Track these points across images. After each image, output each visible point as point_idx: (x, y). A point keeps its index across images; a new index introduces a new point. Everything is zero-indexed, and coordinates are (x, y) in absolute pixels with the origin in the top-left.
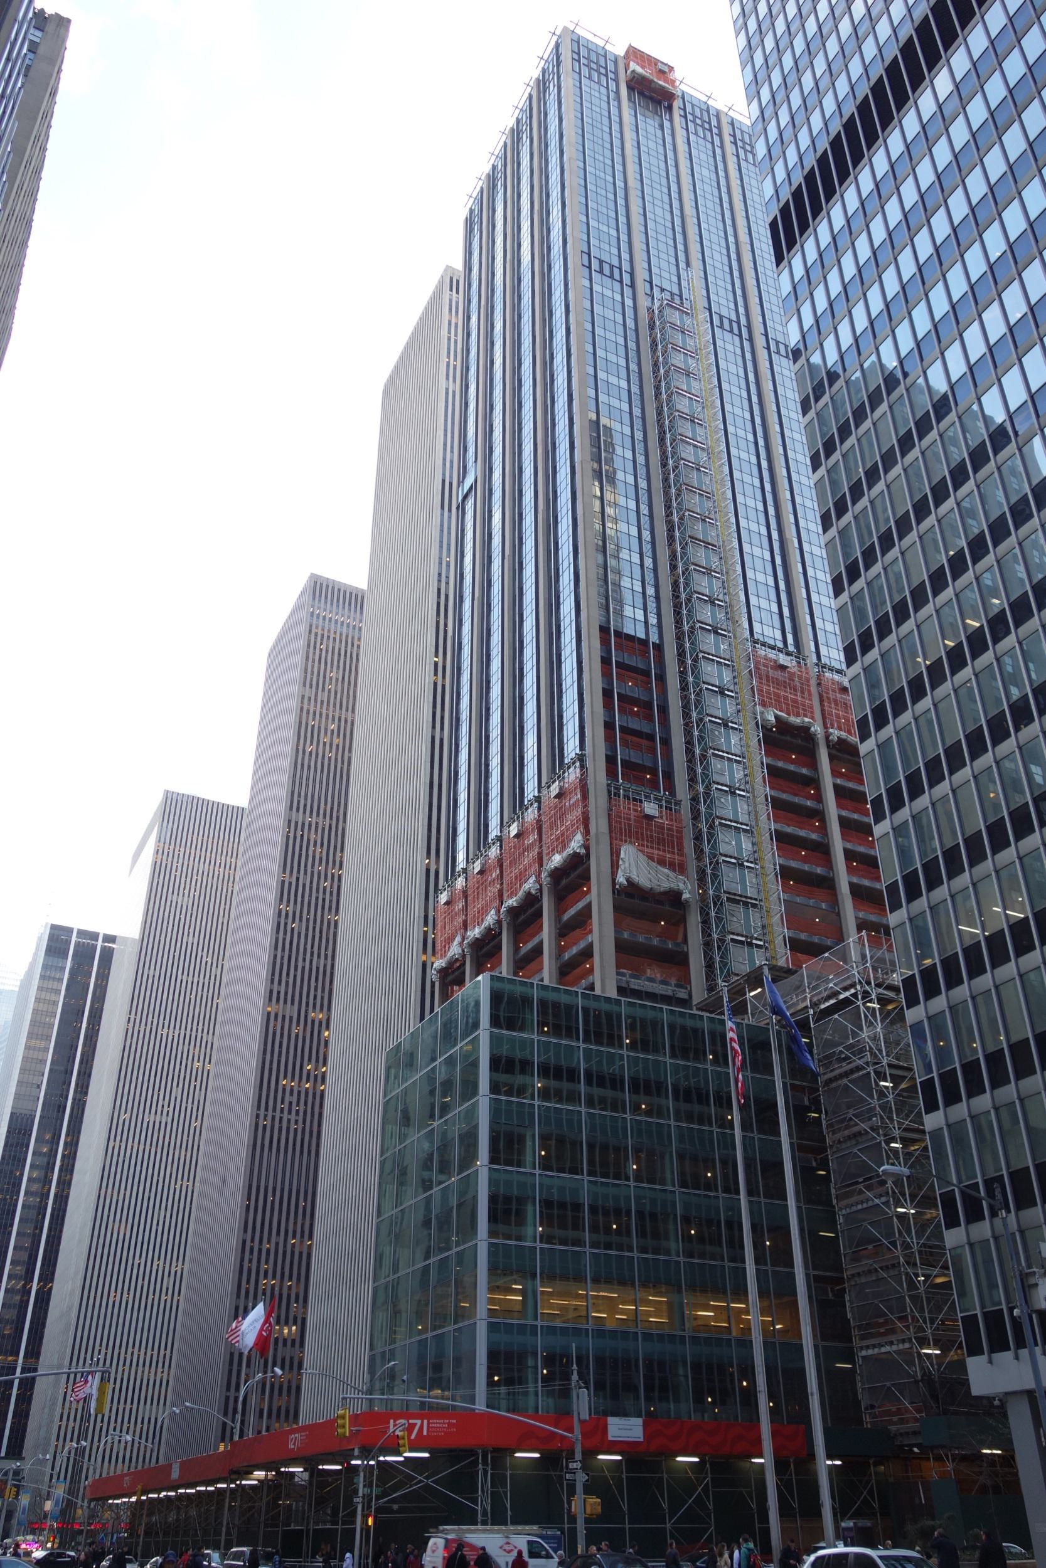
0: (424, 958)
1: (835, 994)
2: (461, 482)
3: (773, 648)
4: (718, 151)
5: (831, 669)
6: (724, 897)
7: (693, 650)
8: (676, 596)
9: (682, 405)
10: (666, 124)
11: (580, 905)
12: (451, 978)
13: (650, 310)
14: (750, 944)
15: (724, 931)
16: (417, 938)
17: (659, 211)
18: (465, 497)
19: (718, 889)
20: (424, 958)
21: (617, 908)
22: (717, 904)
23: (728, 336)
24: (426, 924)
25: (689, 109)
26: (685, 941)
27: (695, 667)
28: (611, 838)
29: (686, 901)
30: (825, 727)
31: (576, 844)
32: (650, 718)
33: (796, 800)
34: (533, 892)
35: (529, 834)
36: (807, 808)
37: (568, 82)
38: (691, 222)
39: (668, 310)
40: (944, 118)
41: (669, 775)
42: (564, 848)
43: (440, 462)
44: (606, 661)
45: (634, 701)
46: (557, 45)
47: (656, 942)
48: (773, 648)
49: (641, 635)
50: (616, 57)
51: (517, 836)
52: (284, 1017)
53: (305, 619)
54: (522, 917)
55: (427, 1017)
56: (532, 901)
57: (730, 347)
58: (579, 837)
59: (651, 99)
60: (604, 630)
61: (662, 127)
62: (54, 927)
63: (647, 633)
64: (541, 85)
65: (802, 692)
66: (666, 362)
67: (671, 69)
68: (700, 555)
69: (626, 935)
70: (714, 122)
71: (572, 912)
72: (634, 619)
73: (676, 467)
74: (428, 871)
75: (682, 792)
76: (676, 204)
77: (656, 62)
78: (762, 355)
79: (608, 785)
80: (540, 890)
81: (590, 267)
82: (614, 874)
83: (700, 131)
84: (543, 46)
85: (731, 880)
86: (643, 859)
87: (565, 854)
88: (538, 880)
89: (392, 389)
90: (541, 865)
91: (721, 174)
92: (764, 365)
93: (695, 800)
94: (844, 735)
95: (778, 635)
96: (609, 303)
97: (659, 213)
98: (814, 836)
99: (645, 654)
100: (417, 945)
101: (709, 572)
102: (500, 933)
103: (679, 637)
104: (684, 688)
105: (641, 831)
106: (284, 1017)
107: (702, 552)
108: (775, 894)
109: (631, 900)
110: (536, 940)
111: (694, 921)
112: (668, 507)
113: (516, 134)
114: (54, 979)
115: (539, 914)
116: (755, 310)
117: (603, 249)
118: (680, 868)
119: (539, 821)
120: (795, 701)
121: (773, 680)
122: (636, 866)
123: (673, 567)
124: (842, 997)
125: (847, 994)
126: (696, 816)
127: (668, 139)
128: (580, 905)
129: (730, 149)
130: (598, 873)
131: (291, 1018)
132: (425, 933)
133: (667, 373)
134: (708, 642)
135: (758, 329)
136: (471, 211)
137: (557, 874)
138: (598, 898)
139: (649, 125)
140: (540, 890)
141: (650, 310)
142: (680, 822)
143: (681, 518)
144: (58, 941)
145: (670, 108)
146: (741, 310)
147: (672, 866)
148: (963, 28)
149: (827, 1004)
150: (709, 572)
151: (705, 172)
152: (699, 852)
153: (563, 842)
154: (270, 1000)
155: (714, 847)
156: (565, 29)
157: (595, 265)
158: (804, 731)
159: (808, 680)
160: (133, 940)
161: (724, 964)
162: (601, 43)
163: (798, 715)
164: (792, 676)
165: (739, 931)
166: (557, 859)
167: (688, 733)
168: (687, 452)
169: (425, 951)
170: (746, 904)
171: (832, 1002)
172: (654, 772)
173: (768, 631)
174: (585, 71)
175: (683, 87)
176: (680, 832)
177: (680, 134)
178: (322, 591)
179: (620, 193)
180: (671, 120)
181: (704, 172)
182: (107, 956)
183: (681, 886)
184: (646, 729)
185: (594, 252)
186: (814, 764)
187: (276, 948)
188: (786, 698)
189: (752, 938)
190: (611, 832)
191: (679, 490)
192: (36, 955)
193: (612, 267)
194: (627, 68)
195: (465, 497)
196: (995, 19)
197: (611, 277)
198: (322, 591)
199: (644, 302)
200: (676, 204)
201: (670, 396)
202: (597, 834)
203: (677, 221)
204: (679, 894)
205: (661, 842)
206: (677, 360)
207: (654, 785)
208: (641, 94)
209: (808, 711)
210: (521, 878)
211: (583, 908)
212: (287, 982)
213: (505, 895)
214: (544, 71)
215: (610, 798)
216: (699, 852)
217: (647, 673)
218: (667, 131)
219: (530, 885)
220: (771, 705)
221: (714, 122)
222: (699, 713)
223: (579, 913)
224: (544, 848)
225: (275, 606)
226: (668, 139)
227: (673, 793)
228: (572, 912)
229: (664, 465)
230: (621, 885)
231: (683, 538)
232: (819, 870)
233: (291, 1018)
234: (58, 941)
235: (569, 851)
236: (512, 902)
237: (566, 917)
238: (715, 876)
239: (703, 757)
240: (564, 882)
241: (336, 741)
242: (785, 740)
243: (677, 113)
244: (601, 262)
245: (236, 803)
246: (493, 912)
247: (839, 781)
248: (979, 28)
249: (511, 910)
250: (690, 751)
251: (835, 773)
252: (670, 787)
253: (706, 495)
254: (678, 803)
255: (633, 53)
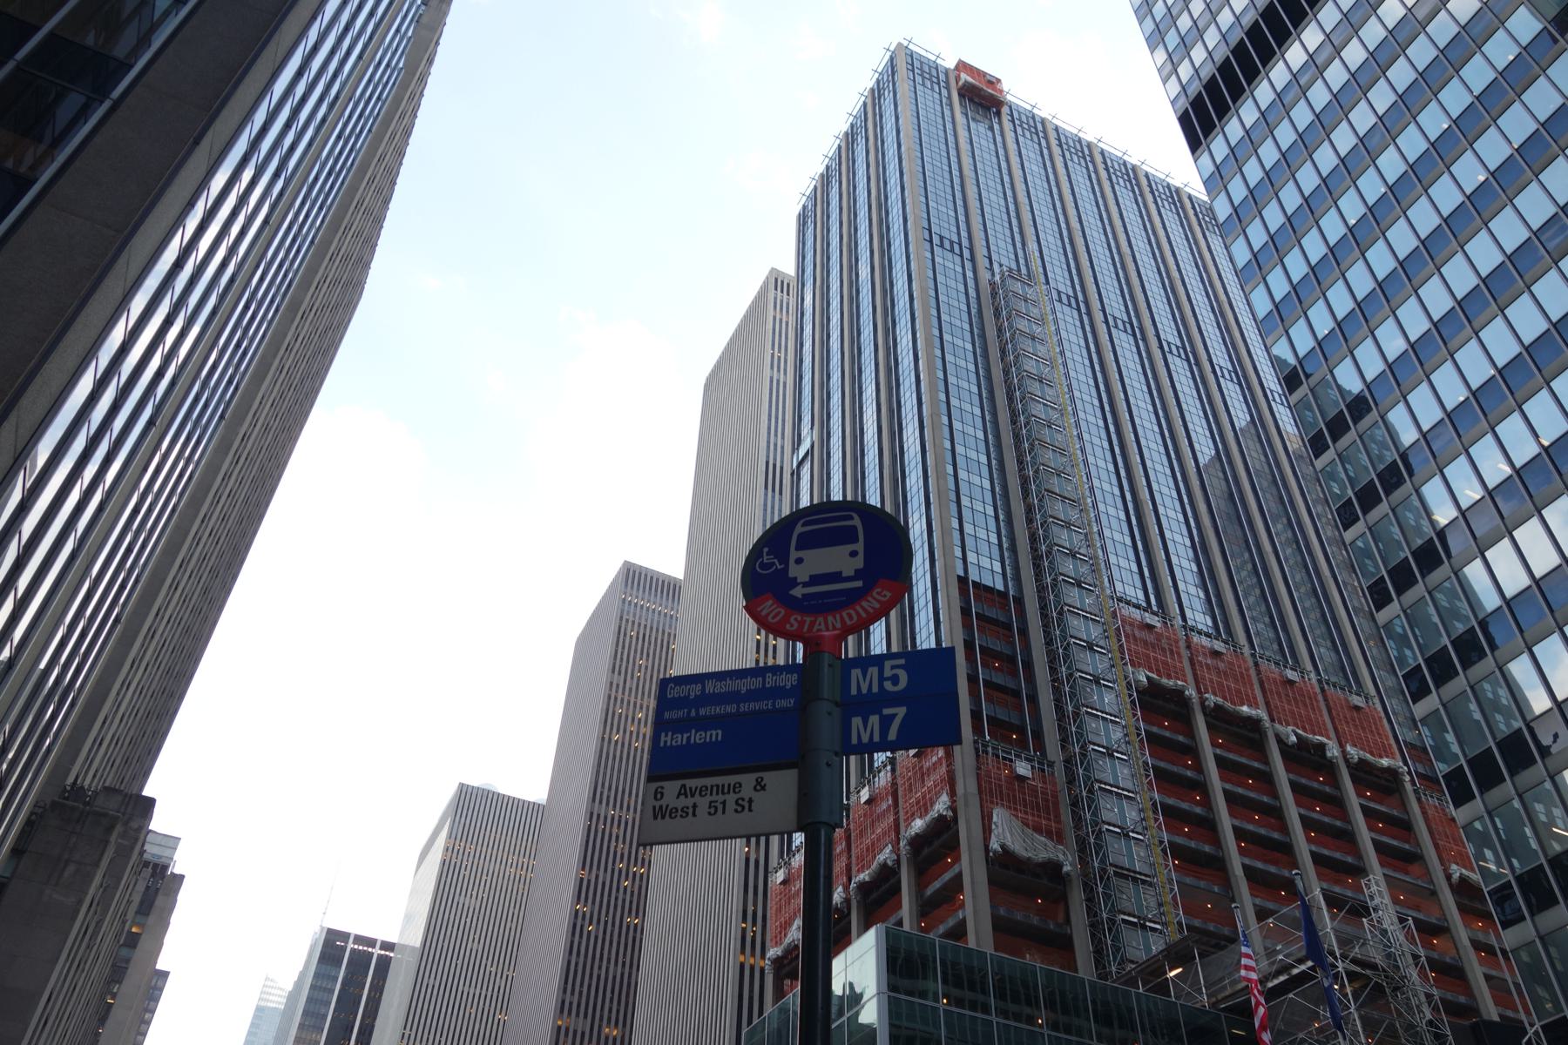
0: (742, 958)
1: (1286, 968)
2: (795, 449)
3: (1137, 607)
4: (1045, 152)
5: (1200, 632)
6: (1111, 870)
7: (1057, 603)
8: (1034, 549)
9: (1030, 366)
10: (996, 127)
11: (947, 876)
12: (784, 971)
13: (992, 284)
14: (1144, 927)
15: (1114, 911)
16: (735, 934)
17: (993, 198)
18: (800, 464)
19: (1102, 861)
20: (742, 958)
21: (992, 882)
22: (1102, 879)
23: (1067, 310)
24: (744, 920)
25: (1016, 115)
26: (1068, 921)
27: (1060, 620)
28: (981, 799)
29: (1068, 874)
30: (1199, 691)
31: (941, 805)
32: (1015, 674)
33: (1175, 769)
34: (890, 863)
35: (882, 799)
36: (1187, 778)
37: (904, 87)
38: (1025, 209)
39: (1009, 281)
40: (1317, 64)
41: (1038, 735)
42: (926, 812)
43: (763, 444)
44: (966, 612)
45: (996, 655)
46: (892, 59)
47: (1035, 920)
48: (1137, 607)
49: (1000, 586)
50: (947, 72)
51: (868, 802)
52: (575, 1032)
53: (617, 603)
54: (874, 895)
55: (755, 1021)
56: (887, 875)
57: (1069, 319)
58: (944, 798)
59: (981, 105)
60: (963, 581)
61: (991, 128)
62: (330, 932)
63: (1006, 585)
64: (876, 94)
65: (1172, 651)
66: (1011, 327)
67: (999, 81)
68: (1058, 509)
69: (1002, 912)
70: (1040, 127)
71: (937, 885)
72: (987, 568)
73: (1027, 424)
74: (747, 860)
75: (1054, 751)
76: (1009, 193)
77: (985, 74)
78: (1102, 329)
79: (975, 742)
80: (898, 861)
81: (931, 241)
82: (987, 840)
83: (1027, 134)
84: (879, 60)
85: (1117, 852)
86: (1017, 824)
87: (928, 818)
88: (896, 850)
89: (715, 384)
90: (897, 832)
91: (1050, 170)
92: (1104, 338)
93: (1068, 762)
94: (1220, 700)
95: (1141, 595)
96: (952, 274)
97: (993, 199)
98: (1198, 810)
99: (1005, 606)
100: (735, 944)
101: (1068, 525)
102: (849, 913)
103: (1041, 589)
104: (1049, 642)
105: (1013, 793)
106: (575, 1032)
107: (1059, 506)
108: (1167, 872)
109: (1004, 867)
110: (956, 869)
111: (1077, 898)
112: (1020, 462)
113: (825, 179)
114: (325, 989)
115: (897, 889)
116: (1091, 288)
117: (945, 226)
118: (1059, 838)
119: (894, 784)
120: (1165, 663)
121: (1142, 642)
122: (1007, 831)
123: (1030, 521)
124: (1295, 971)
125: (1303, 967)
126: (1071, 780)
127: (999, 139)
128: (947, 876)
129: (1056, 150)
130: (969, 838)
131: (583, 1034)
132: (744, 930)
133: (1013, 336)
134: (1073, 596)
135: (1096, 305)
136: (804, 207)
137: (918, 842)
138: (970, 868)
139: (980, 129)
140: (898, 861)
141: (992, 284)
142: (1055, 784)
143: (1037, 471)
144: (332, 947)
145: (998, 114)
146: (1078, 288)
147: (1049, 835)
148: (1206, 137)
149: (1276, 982)
150: (1068, 525)
151: (1035, 168)
152: (1078, 821)
153: (924, 807)
154: (562, 1011)
155: (1095, 814)
156: (900, 44)
157: (936, 240)
158: (1178, 694)
159: (1177, 642)
160: (413, 948)
161: (1117, 949)
162: (933, 58)
163: (1169, 677)
164: (1159, 637)
165: (1130, 910)
166: (918, 824)
167: (1057, 691)
168: (1037, 410)
169: (743, 952)
170: (1135, 880)
171: (1282, 978)
172: (1021, 731)
173: (1130, 592)
174: (919, 79)
175: (1009, 97)
176: (1055, 796)
177: (1010, 136)
178: (634, 578)
179: (957, 181)
180: (1000, 123)
181: (1034, 168)
182: (384, 965)
183: (1061, 857)
184: (1011, 685)
185: (934, 229)
186: (1190, 731)
187: (571, 953)
188: (1156, 659)
189: (1146, 919)
190: (980, 792)
191: (1032, 445)
192: (302, 975)
193: (952, 243)
194: (958, 79)
195: (800, 464)
196: (1328, 15)
197: (952, 250)
198: (634, 578)
199: (985, 276)
200: (1009, 193)
201: (1016, 357)
202: (965, 795)
203: (1012, 207)
204: (1059, 866)
205: (1037, 808)
206: (1022, 325)
207: (1022, 743)
208: (971, 100)
209: (1180, 674)
210: (873, 849)
211: (951, 880)
212: (581, 993)
213: (854, 869)
214: (852, 126)
215: (978, 756)
216: (1078, 821)
217: (1009, 627)
218: (997, 132)
219: (885, 855)
220: (1140, 665)
221: (1040, 127)
222: (1069, 668)
223: (945, 887)
224: (901, 814)
225: (590, 587)
226: (999, 139)
227: (1044, 754)
228: (937, 885)
229: (1014, 422)
230: (995, 852)
231: (1039, 492)
232: (1207, 848)
233: (583, 1034)
234: (332, 947)
235: (933, 814)
236: (864, 876)
237: (929, 891)
238: (1099, 847)
239: (1076, 715)
240: (926, 851)
241: (643, 730)
242: (1159, 704)
243: (1005, 119)
244: (942, 238)
245: (532, 799)
246: (840, 889)
247: (1218, 751)
248: (1235, 120)
249: (862, 886)
250: (1059, 708)
251: (1214, 744)
252: (1040, 745)
253: (1061, 451)
254: (1051, 764)
255: (962, 66)
